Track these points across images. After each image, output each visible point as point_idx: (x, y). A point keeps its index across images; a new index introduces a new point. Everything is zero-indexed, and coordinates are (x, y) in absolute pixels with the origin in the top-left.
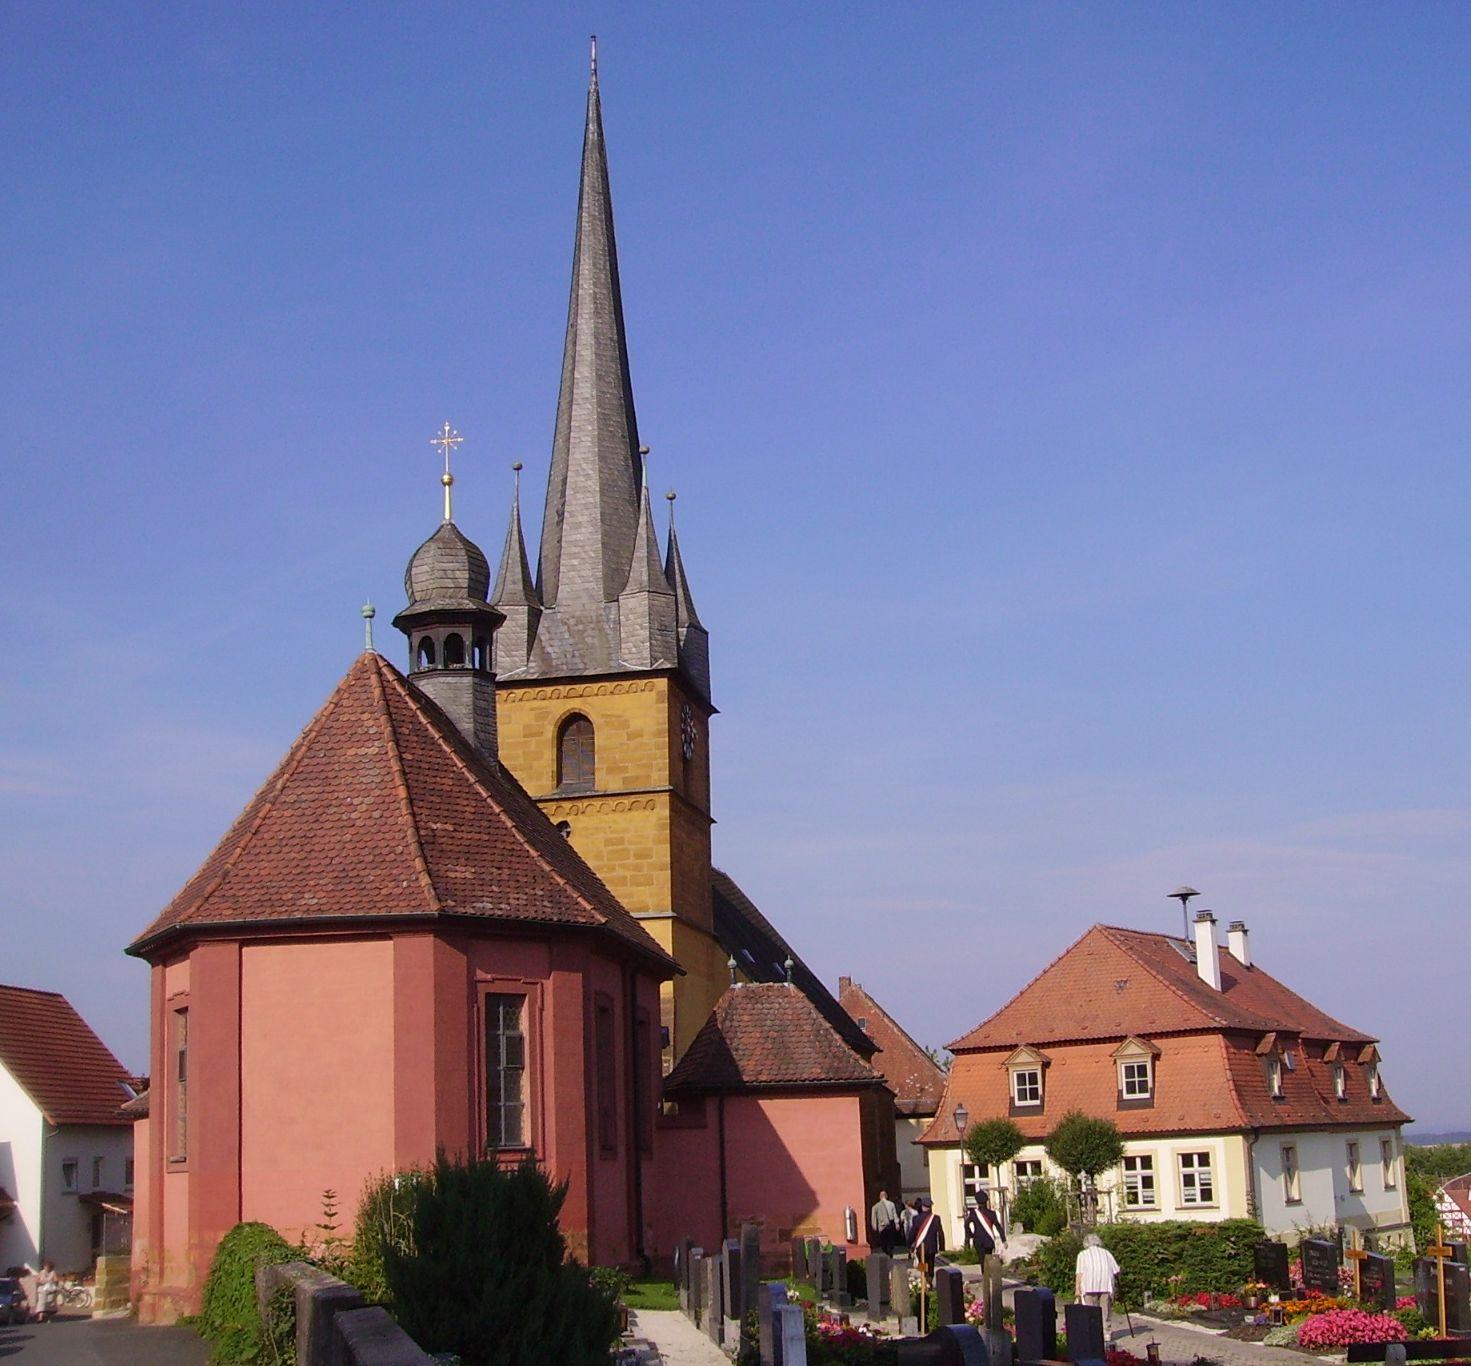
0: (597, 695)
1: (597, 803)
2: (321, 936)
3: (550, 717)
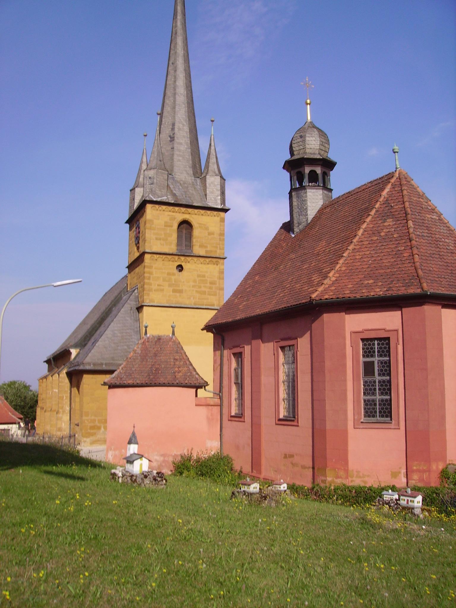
1: (195, 259)
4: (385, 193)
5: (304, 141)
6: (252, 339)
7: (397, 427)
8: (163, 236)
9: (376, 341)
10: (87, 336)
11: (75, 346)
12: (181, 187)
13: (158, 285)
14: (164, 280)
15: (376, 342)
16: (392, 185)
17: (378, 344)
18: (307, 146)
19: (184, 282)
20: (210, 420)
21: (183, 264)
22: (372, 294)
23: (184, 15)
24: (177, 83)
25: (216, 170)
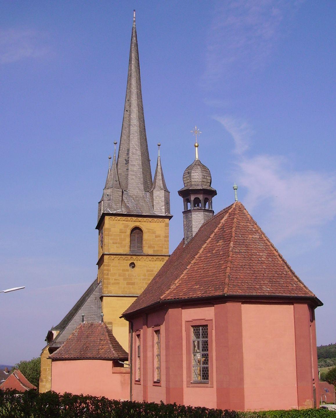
0: (145, 222)
1: (145, 257)
2: (273, 302)
3: (129, 227)
4: (223, 221)
5: (190, 176)
6: (143, 325)
7: (211, 386)
8: (119, 241)
9: (201, 327)
10: (66, 320)
11: (56, 328)
12: (133, 201)
13: (115, 280)
14: (120, 275)
15: (201, 328)
16: (229, 214)
17: (202, 329)
18: (193, 180)
19: (136, 276)
20: (123, 384)
21: (135, 262)
22: (195, 296)
23: (138, 60)
24: (131, 117)
25: (162, 185)
